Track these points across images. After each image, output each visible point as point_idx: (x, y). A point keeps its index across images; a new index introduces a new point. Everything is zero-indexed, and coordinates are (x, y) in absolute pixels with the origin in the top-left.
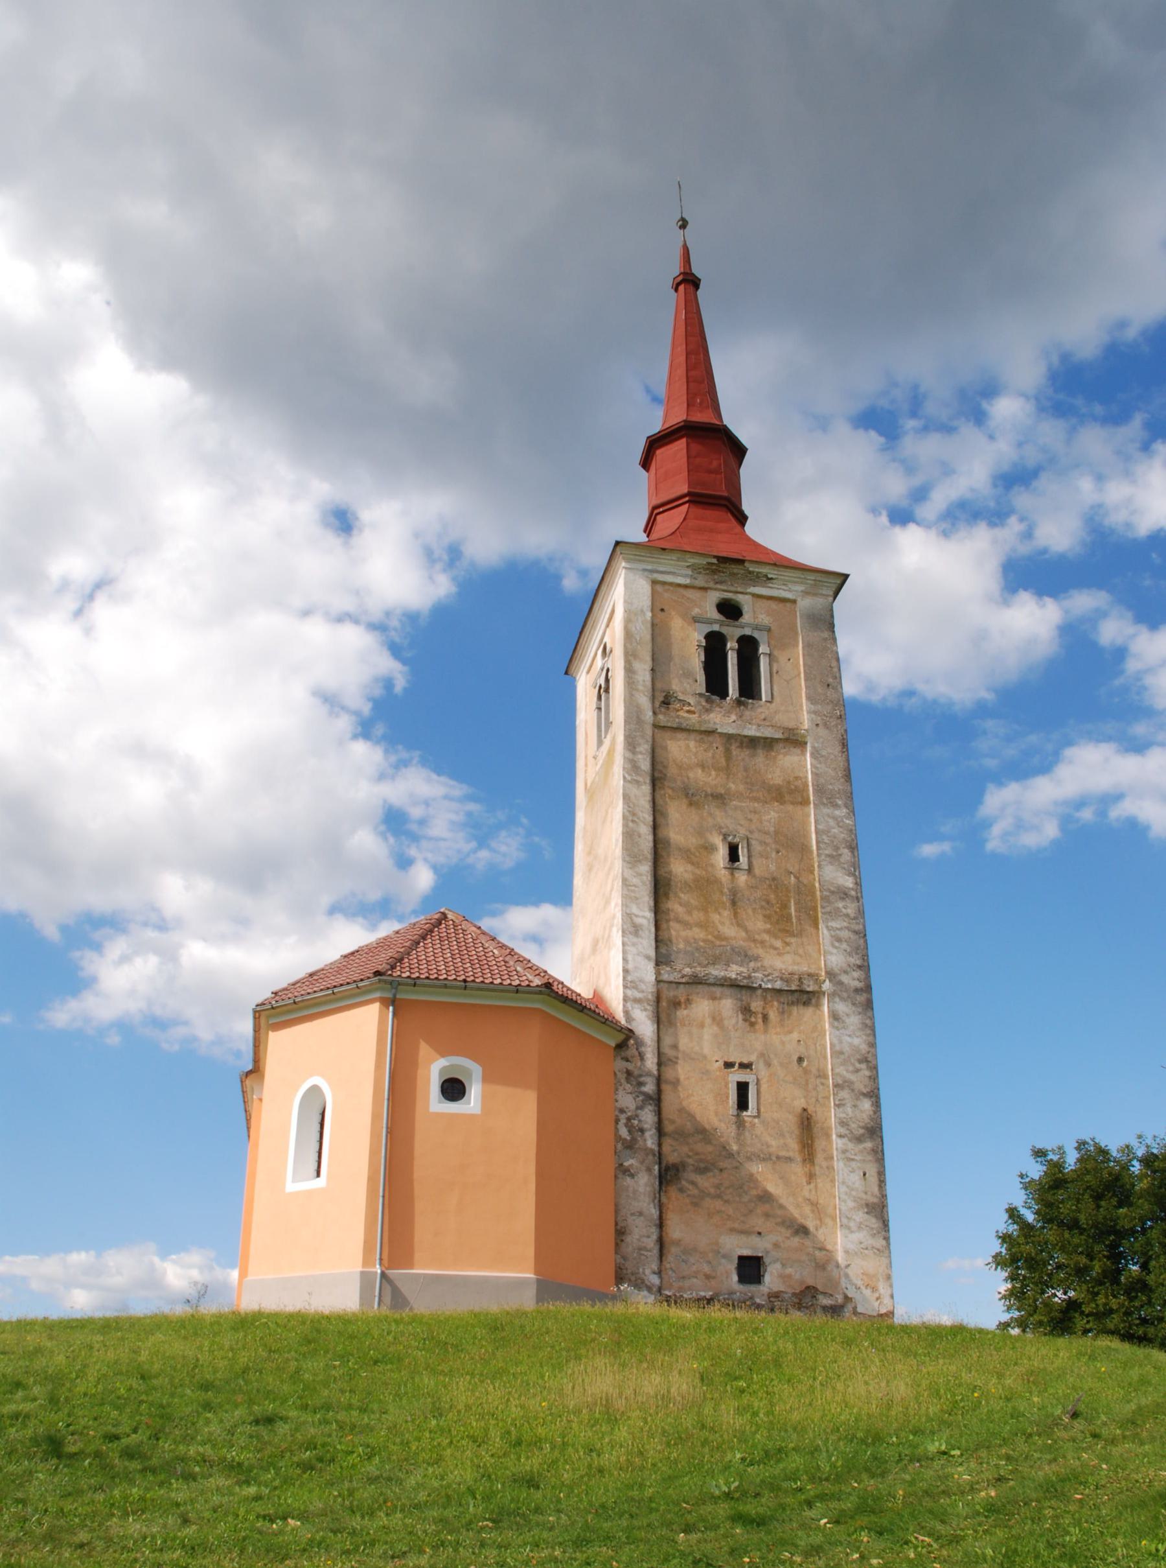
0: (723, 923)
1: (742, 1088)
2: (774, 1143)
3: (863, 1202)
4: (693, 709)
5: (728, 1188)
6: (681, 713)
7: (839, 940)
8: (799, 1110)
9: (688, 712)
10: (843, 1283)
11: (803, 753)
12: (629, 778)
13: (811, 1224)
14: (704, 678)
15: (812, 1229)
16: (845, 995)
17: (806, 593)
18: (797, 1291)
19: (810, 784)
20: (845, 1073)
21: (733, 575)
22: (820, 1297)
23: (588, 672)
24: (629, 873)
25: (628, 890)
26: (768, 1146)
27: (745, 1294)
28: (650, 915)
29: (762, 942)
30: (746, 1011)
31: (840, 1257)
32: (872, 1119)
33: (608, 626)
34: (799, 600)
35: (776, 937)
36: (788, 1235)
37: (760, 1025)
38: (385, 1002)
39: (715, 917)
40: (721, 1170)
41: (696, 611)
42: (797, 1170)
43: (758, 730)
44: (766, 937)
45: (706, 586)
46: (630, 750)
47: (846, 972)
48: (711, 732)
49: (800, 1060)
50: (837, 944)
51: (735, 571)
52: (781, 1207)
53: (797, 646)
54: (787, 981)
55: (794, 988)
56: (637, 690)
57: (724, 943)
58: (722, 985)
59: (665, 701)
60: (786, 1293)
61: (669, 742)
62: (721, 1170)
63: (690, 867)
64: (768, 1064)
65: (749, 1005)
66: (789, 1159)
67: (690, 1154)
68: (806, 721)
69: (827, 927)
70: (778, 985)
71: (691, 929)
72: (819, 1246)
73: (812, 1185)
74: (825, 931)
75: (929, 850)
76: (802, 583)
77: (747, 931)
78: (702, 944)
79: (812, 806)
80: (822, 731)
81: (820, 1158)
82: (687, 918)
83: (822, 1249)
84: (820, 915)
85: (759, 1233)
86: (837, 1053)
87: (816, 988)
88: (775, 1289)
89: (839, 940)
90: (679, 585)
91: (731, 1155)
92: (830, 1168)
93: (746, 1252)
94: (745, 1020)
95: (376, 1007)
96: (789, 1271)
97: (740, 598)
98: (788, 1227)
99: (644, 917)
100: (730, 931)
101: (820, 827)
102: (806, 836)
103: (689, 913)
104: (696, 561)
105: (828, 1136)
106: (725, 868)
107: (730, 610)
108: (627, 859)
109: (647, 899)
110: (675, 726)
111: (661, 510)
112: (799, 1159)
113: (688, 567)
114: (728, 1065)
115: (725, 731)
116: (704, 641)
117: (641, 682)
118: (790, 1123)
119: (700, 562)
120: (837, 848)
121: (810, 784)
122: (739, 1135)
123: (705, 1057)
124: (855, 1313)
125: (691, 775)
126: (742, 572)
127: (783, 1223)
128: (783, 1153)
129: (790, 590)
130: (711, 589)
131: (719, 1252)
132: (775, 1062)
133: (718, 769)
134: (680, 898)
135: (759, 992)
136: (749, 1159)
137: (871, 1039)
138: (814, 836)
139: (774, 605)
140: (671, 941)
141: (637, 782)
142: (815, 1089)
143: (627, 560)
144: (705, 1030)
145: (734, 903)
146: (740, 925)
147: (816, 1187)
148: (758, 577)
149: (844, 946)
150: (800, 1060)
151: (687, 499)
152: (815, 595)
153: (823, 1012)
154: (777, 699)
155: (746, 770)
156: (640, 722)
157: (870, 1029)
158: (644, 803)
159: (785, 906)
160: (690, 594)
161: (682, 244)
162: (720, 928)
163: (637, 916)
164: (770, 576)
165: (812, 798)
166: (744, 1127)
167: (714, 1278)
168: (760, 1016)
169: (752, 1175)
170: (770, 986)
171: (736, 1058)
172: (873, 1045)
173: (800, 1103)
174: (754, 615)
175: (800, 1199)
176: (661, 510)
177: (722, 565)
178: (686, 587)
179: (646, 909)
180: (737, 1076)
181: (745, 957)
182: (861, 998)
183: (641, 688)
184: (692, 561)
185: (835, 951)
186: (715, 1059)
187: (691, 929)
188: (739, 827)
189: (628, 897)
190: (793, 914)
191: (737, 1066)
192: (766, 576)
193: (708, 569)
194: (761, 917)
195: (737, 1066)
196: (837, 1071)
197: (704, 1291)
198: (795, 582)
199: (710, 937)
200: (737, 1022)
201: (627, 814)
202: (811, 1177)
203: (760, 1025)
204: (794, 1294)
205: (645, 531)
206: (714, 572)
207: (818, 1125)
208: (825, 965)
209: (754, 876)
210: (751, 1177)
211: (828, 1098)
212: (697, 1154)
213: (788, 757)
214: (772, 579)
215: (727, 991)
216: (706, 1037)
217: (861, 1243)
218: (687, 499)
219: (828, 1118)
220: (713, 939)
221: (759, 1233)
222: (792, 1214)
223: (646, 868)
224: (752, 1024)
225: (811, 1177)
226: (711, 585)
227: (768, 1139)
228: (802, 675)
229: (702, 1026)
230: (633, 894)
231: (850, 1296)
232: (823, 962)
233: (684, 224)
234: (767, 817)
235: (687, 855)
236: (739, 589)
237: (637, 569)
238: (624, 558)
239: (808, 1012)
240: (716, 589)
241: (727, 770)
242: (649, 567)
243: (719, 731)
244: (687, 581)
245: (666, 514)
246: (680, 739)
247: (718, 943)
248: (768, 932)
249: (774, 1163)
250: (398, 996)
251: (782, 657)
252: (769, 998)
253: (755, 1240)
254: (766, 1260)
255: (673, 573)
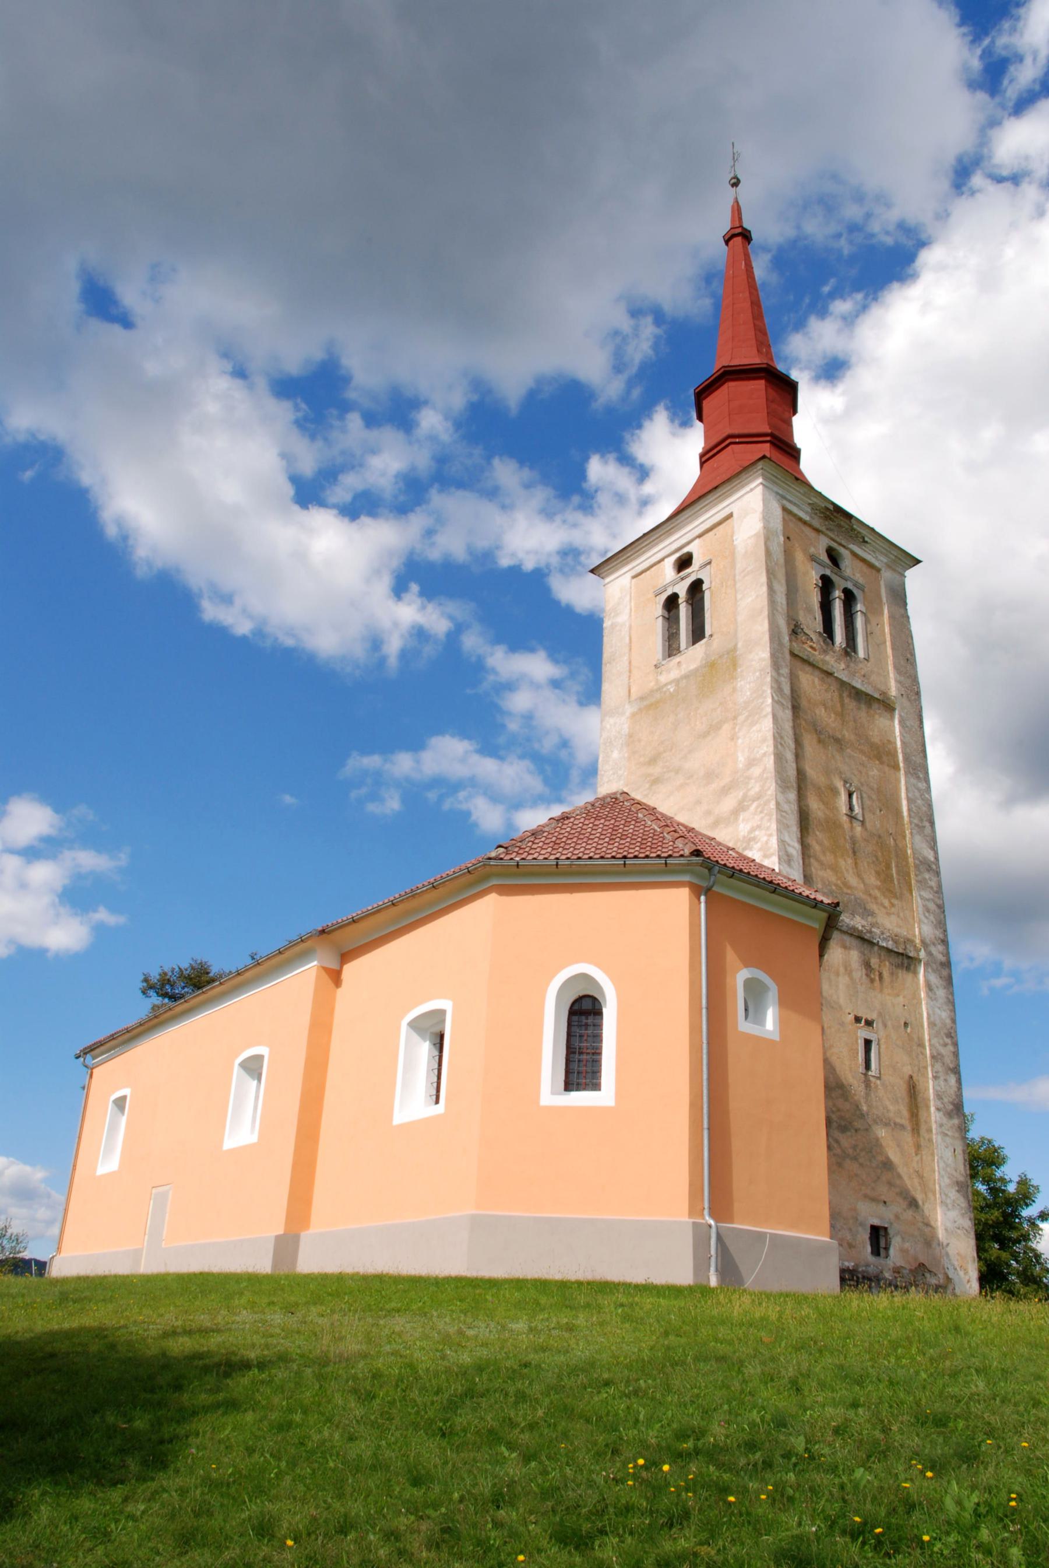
0: (847, 870)
1: (868, 1043)
2: (891, 1108)
3: (955, 1179)
4: (815, 645)
5: (862, 1150)
6: (805, 646)
7: (928, 911)
8: (907, 1077)
9: (811, 647)
10: (945, 1261)
11: (892, 718)
12: (776, 698)
13: (919, 1197)
14: (821, 618)
15: (920, 1203)
16: (934, 966)
17: (889, 566)
18: (913, 1268)
19: (900, 751)
20: (937, 1045)
21: (840, 526)
22: (928, 1275)
23: (634, 577)
24: (781, 797)
25: (782, 816)
26: (888, 1111)
27: (877, 1267)
28: (798, 846)
29: (876, 898)
30: (867, 965)
31: (941, 1234)
32: (957, 1095)
33: (700, 536)
34: (883, 569)
35: (885, 897)
36: (905, 1207)
37: (877, 983)
38: (697, 891)
39: (842, 863)
40: (856, 1131)
41: (812, 550)
42: (907, 1137)
43: (863, 685)
44: (877, 893)
45: (820, 529)
46: (775, 669)
47: (934, 944)
48: (830, 674)
49: (906, 1024)
50: (927, 914)
51: (842, 523)
52: (899, 1176)
53: (882, 613)
54: (896, 942)
55: (901, 951)
56: (777, 610)
57: (849, 891)
58: (851, 935)
59: (796, 631)
60: (905, 1268)
61: (800, 673)
62: (856, 1131)
63: (822, 807)
64: (885, 1026)
65: (869, 959)
66: (902, 1127)
67: (834, 1109)
68: (893, 691)
69: (920, 895)
70: (890, 945)
71: (825, 870)
72: (925, 1221)
73: (919, 1156)
74: (919, 900)
75: (288, 799)
76: (886, 555)
77: (865, 884)
78: (834, 888)
79: (902, 772)
80: (904, 700)
81: (923, 1128)
82: (822, 858)
83: (928, 1225)
84: (913, 882)
85: (885, 1202)
86: (932, 1024)
87: (915, 955)
88: (898, 1264)
89: (928, 911)
90: (800, 519)
91: (862, 1116)
92: (930, 1140)
93: (876, 1222)
94: (867, 975)
95: (684, 893)
96: (907, 1245)
97: (842, 550)
98: (905, 1198)
99: (793, 847)
100: (853, 881)
101: (910, 795)
102: (898, 800)
103: (824, 852)
104: (818, 501)
105: (928, 1107)
106: (847, 815)
107: (833, 557)
108: (779, 782)
109: (795, 829)
110: (805, 657)
111: (737, 440)
112: (909, 1128)
113: (809, 504)
114: (858, 1020)
115: (840, 677)
116: (820, 581)
117: (779, 604)
118: (902, 1090)
119: (820, 504)
120: (921, 820)
121: (900, 751)
122: (867, 1095)
123: (840, 1007)
124: (954, 1294)
125: (817, 712)
126: (847, 527)
127: (900, 1194)
128: (898, 1120)
129: (876, 558)
130: (823, 533)
131: (857, 1220)
132: (889, 1023)
133: (836, 714)
134: (816, 835)
135: (876, 948)
136: (875, 1122)
137: (952, 1014)
138: (904, 803)
139: (865, 568)
140: (812, 878)
141: (783, 704)
142: (917, 1057)
143: (765, 478)
144: (840, 978)
145: (854, 853)
146: (859, 876)
147: (922, 1159)
148: (857, 537)
149: (932, 918)
150: (906, 1024)
151: (768, 439)
152: (894, 570)
153: (918, 980)
154: (872, 660)
155: (855, 721)
156: (781, 644)
157: (951, 1003)
158: (788, 726)
159: (888, 867)
160: (808, 531)
161: (731, 202)
162: (846, 875)
163: (789, 845)
164: (866, 539)
165: (901, 765)
166: (870, 1087)
167: (854, 1247)
168: (877, 973)
169: (877, 1139)
170: (884, 944)
171: (865, 1015)
172: (954, 1021)
173: (907, 1070)
174: (851, 571)
175: (911, 1171)
176: (737, 440)
177: (835, 514)
178: (805, 523)
179: (795, 840)
180: (863, 1033)
181: (867, 913)
182: (945, 973)
183: (779, 609)
184: (815, 500)
185: (926, 921)
186: (848, 1011)
187: (825, 870)
188: (853, 776)
189: (782, 826)
190: (895, 875)
191: (863, 1021)
192: (864, 538)
193: (823, 513)
194: (873, 872)
195: (863, 1021)
196: (933, 1042)
197: (847, 1261)
198: (882, 553)
199: (839, 882)
200: (862, 976)
201: (776, 735)
202: (918, 1147)
203: (877, 983)
204: (911, 1270)
205: (702, 456)
206: (827, 518)
207: (921, 1095)
208: (920, 933)
209: (866, 829)
210: (877, 1143)
211: (926, 1068)
212: (839, 1110)
213: (881, 719)
214: (867, 542)
215: (854, 942)
216: (841, 986)
217: (955, 1222)
218: (768, 439)
219: (927, 1089)
220: (842, 886)
221: (885, 1202)
222: (906, 1185)
223: (792, 796)
224: (872, 981)
225: (918, 1147)
226: (823, 529)
227: (888, 1103)
228: (888, 644)
229: (837, 974)
230: (785, 821)
231: (950, 1276)
232: (917, 930)
233: (736, 183)
234: (871, 773)
235: (820, 792)
236: (843, 542)
237: (772, 490)
238: (763, 475)
239: (909, 977)
240: (826, 535)
241: (841, 715)
242: (780, 492)
243: (836, 675)
244: (807, 518)
245: (741, 446)
246: (807, 673)
247: (845, 890)
248: (879, 888)
249: (893, 1129)
250: (714, 889)
251: (874, 620)
252: (883, 957)
253: (881, 1208)
254: (891, 1232)
255: (795, 504)
